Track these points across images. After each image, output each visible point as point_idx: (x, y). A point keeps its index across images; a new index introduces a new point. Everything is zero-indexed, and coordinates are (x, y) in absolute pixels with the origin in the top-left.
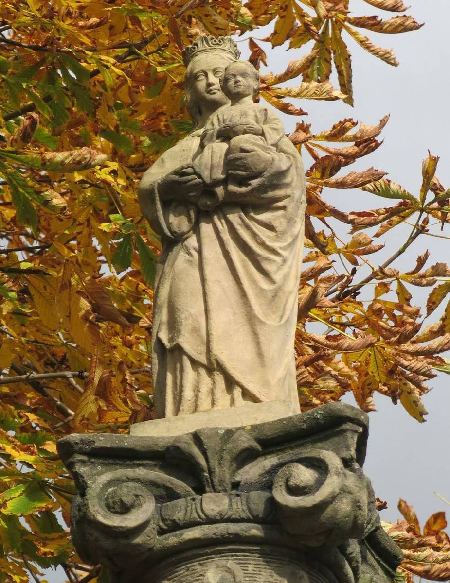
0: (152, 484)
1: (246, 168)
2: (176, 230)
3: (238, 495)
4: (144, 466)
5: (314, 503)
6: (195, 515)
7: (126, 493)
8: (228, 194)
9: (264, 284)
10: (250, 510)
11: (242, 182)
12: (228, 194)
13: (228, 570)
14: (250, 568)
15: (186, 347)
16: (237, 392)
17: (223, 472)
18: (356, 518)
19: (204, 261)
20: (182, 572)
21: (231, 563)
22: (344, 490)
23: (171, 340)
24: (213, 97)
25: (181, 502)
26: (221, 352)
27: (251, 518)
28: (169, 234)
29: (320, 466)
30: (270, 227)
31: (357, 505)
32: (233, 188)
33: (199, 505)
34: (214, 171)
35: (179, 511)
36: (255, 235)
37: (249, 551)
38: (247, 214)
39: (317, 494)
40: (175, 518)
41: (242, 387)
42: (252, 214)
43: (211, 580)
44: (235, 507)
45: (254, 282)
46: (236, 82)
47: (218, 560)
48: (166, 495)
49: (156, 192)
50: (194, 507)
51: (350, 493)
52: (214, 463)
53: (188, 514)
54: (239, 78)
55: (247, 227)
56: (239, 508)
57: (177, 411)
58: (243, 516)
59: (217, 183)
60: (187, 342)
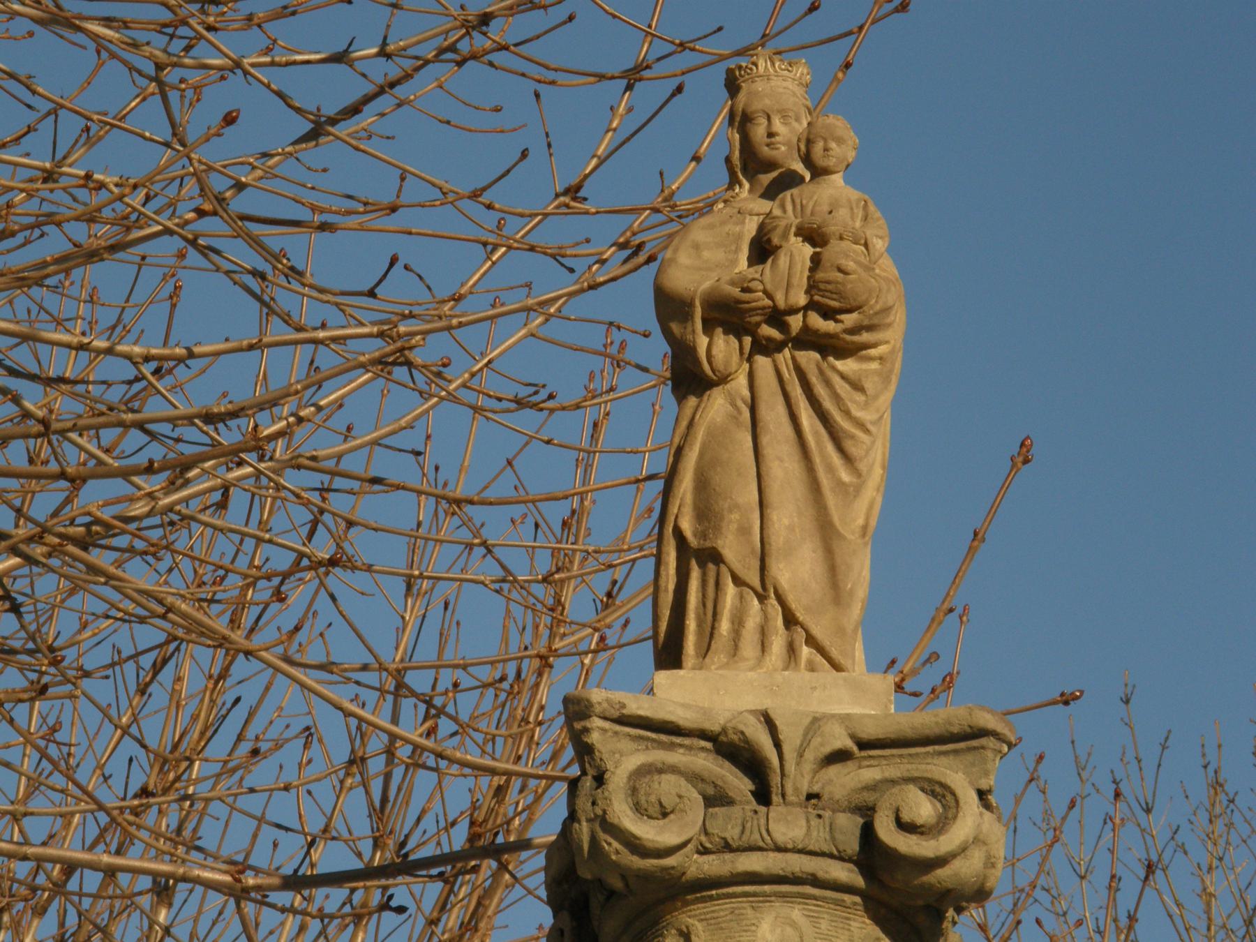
0: (695, 778)
1: (840, 295)
2: (721, 368)
3: (819, 816)
4: (689, 748)
5: (938, 854)
6: (757, 836)
7: (668, 787)
8: (806, 328)
9: (845, 476)
10: (833, 839)
11: (828, 314)
12: (806, 328)
13: (793, 924)
14: (824, 925)
15: (729, 553)
16: (800, 635)
17: (799, 776)
18: (985, 877)
19: (760, 425)
20: (722, 914)
21: (796, 913)
22: (977, 840)
23: (703, 535)
24: (774, 153)
25: (736, 811)
26: (782, 574)
27: (835, 852)
28: (709, 373)
29: (939, 791)
30: (857, 387)
31: (990, 863)
32: (816, 321)
33: (763, 821)
34: (792, 292)
35: (728, 825)
36: (837, 397)
37: (823, 899)
38: (824, 357)
39: (942, 838)
40: (728, 836)
41: (806, 631)
42: (831, 359)
43: (769, 936)
44: (815, 834)
45: (830, 469)
46: (826, 150)
47: (779, 907)
48: (716, 799)
49: (697, 303)
50: (755, 822)
51: (985, 843)
52: (791, 766)
53: (747, 832)
54: (833, 145)
55: (828, 383)
56: (819, 839)
57: (705, 650)
58: (826, 848)
59: (793, 311)
60: (731, 547)
